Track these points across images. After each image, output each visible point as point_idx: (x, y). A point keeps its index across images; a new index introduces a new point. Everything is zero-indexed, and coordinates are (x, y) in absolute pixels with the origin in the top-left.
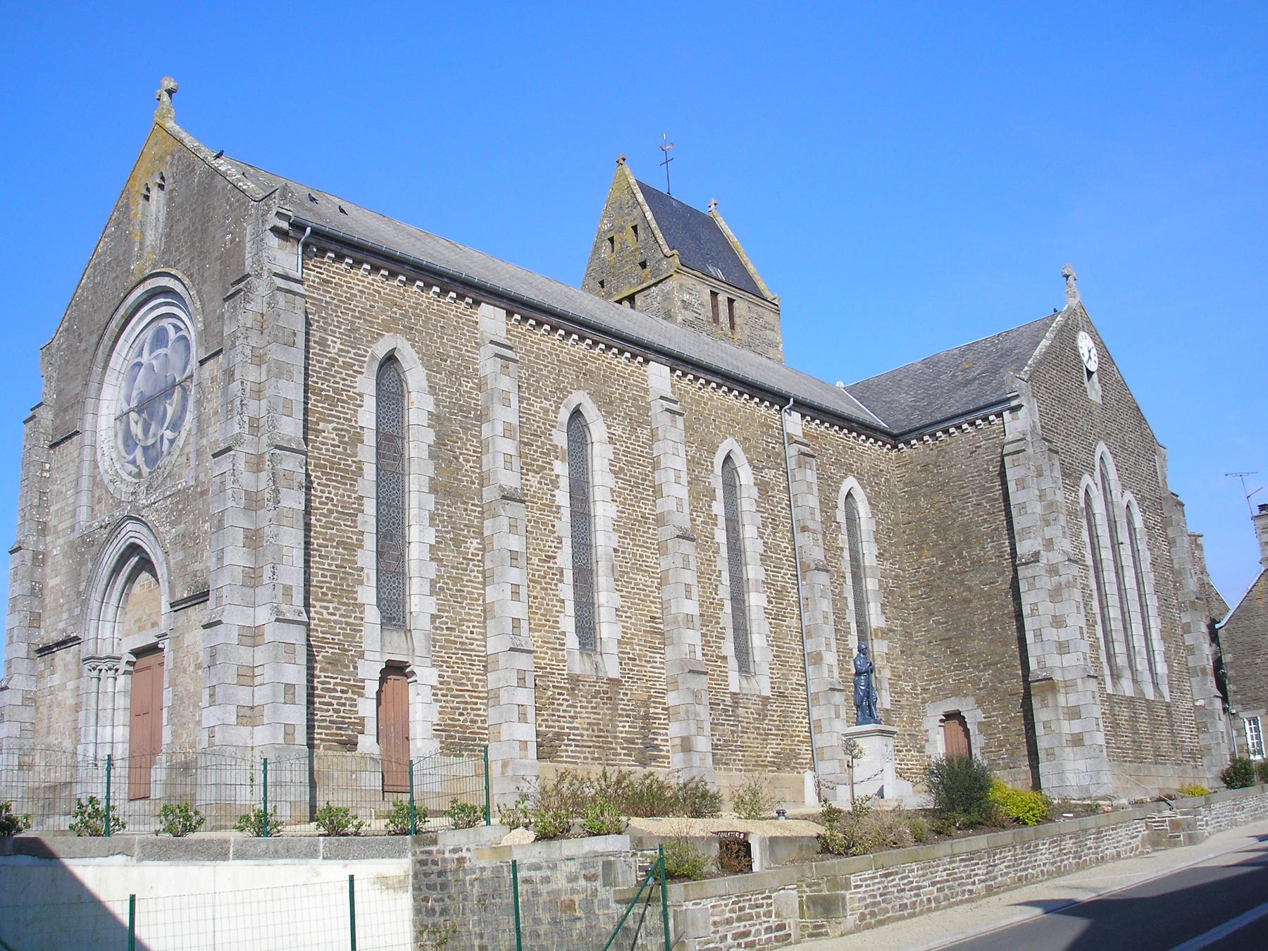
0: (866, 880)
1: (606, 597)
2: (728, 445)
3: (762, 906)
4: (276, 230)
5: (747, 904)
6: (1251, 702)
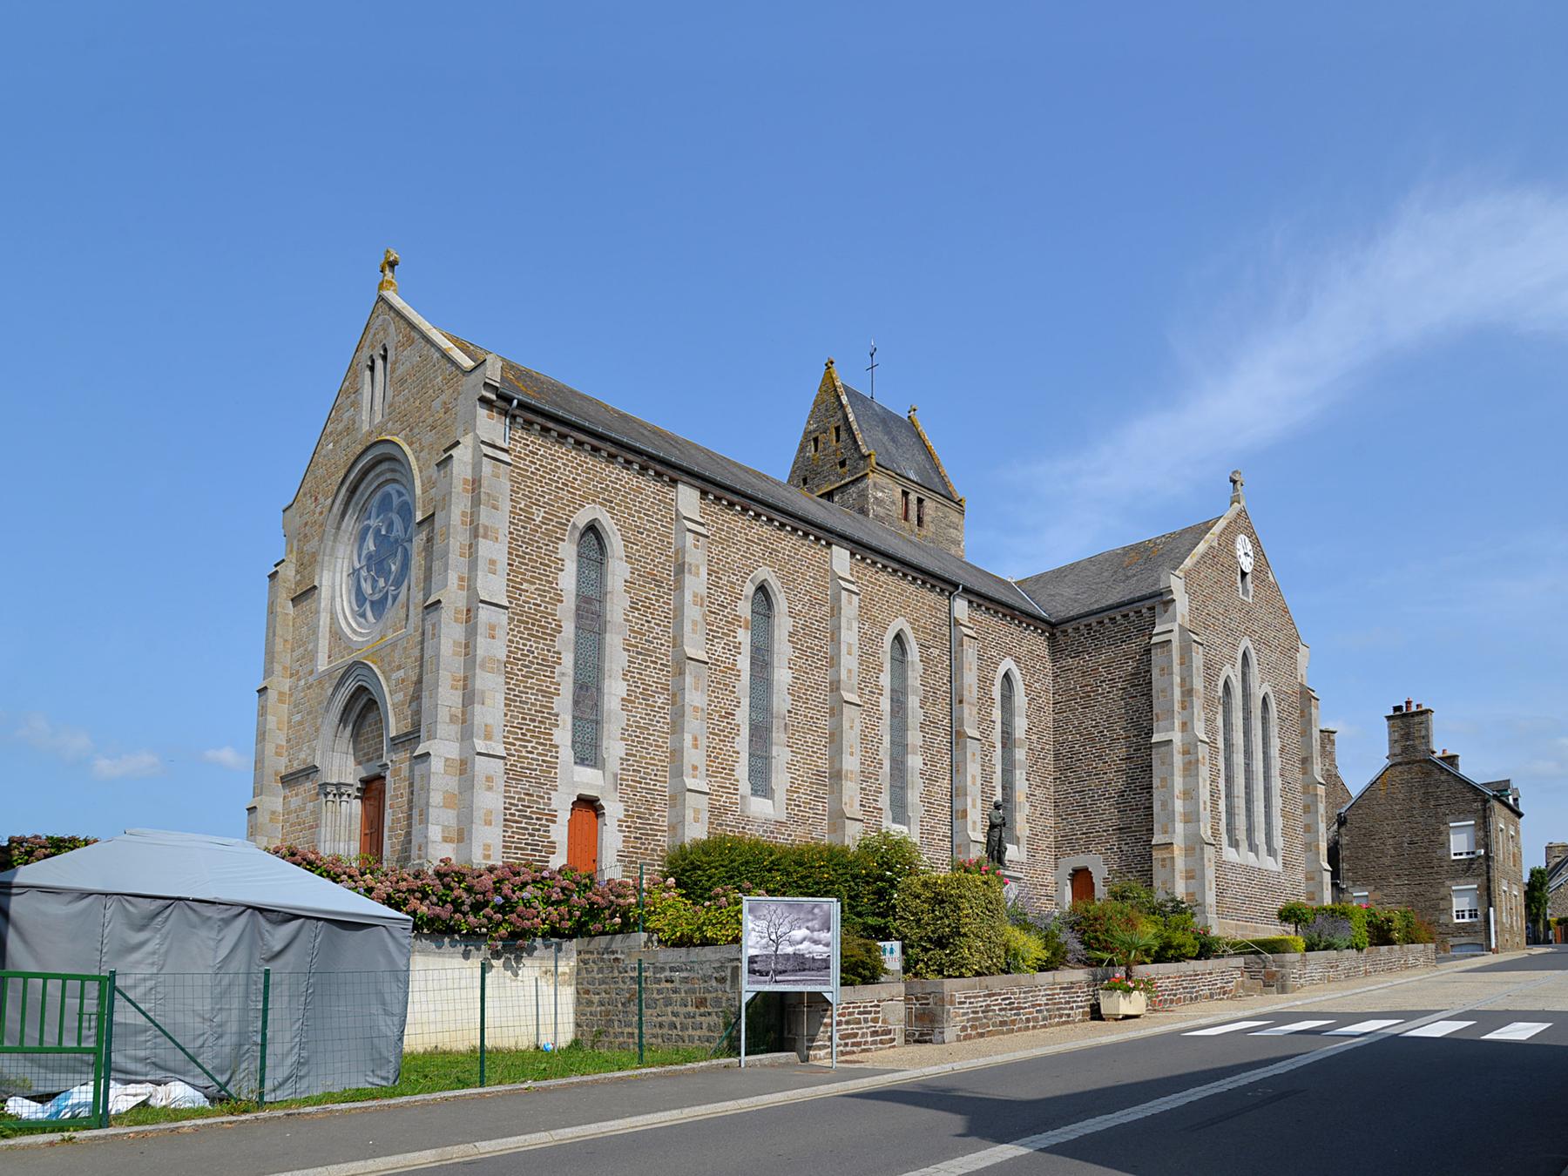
1: (781, 754)
2: (1008, 664)
4: (483, 400)
6: (1364, 880)
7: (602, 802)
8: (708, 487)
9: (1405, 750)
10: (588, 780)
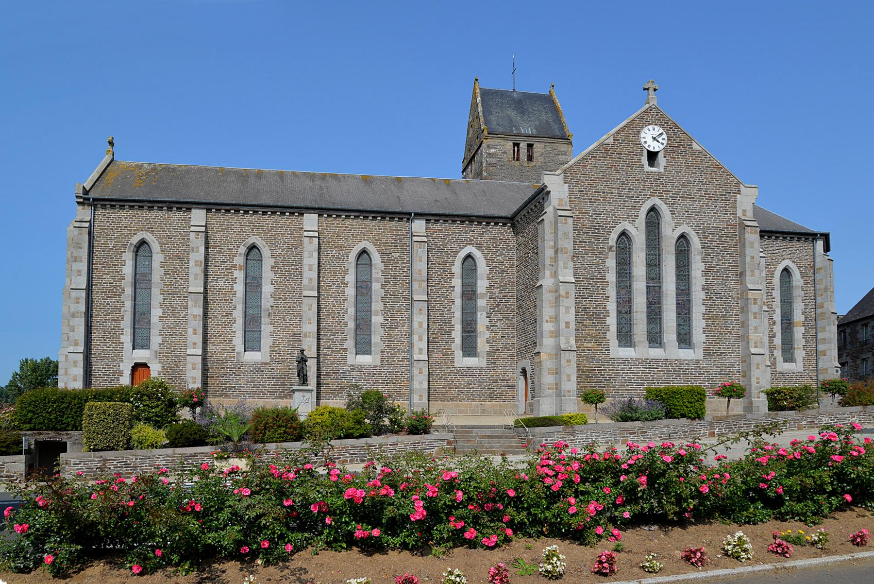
1: (266, 329)
10: (141, 355)
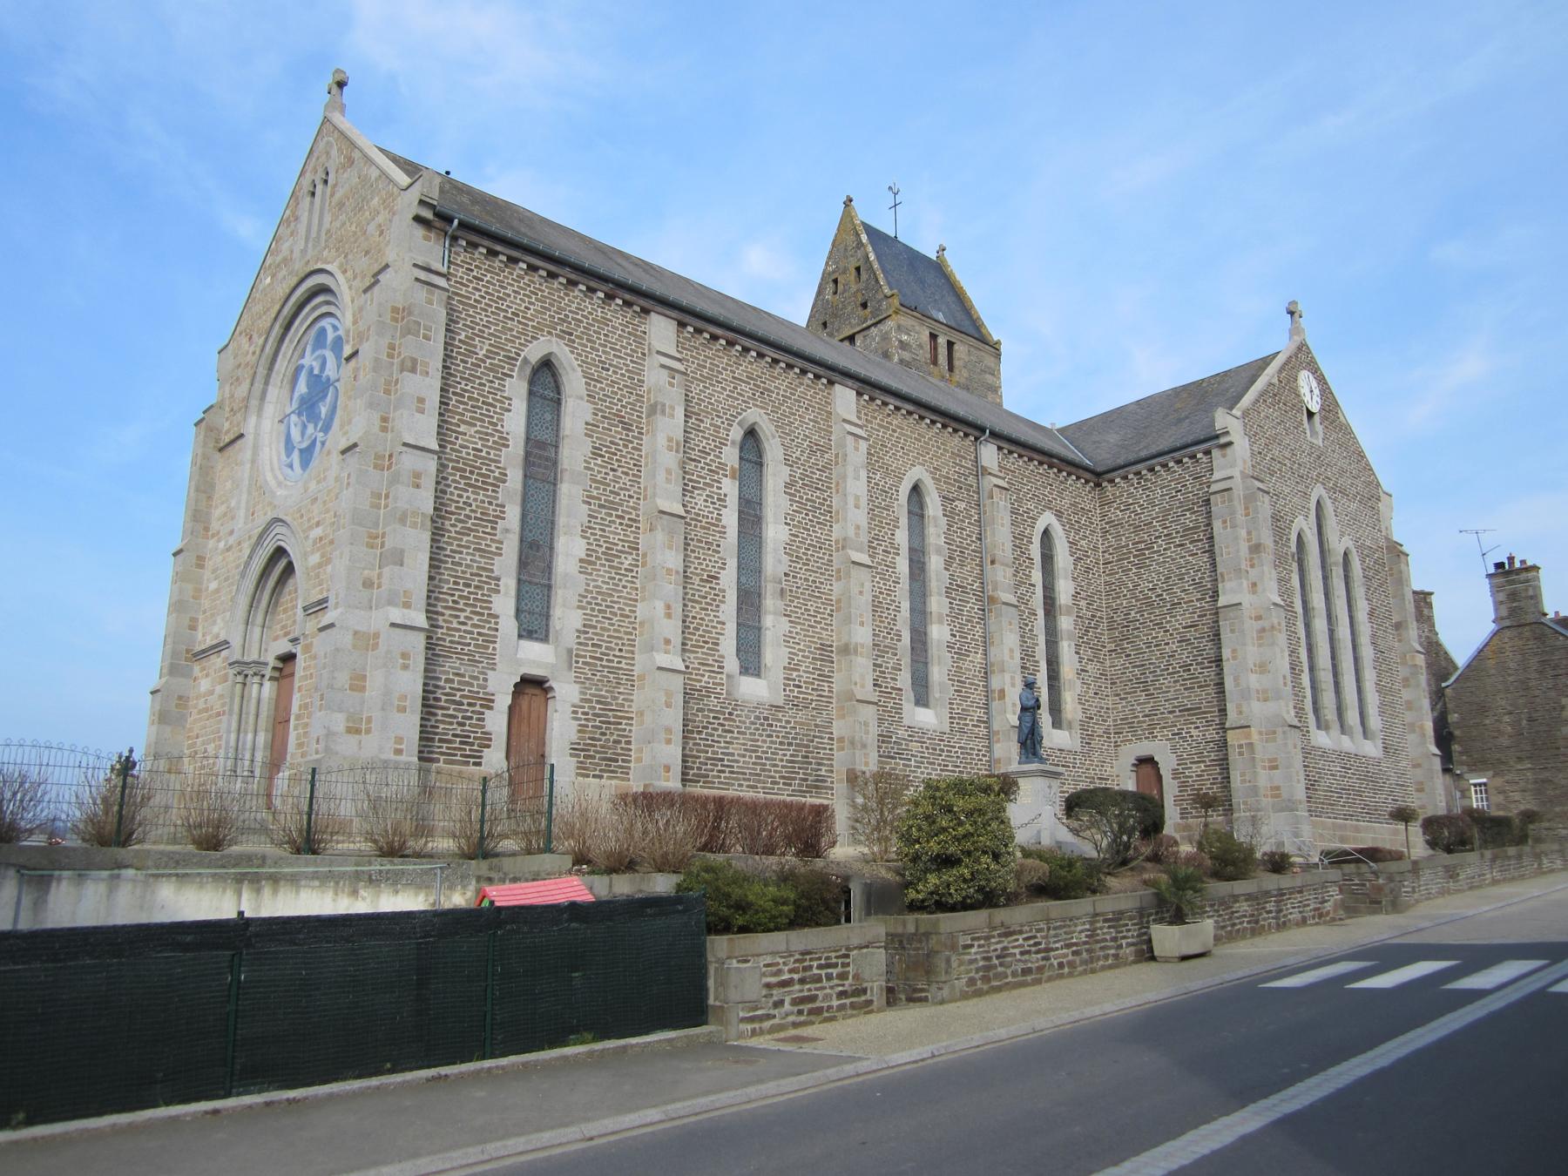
0: (978, 939)
1: (774, 624)
2: (1047, 519)
3: (835, 966)
4: (418, 219)
5: (815, 964)
6: (1477, 766)
7: (552, 683)
8: (687, 319)
9: (1513, 612)
10: (536, 657)
